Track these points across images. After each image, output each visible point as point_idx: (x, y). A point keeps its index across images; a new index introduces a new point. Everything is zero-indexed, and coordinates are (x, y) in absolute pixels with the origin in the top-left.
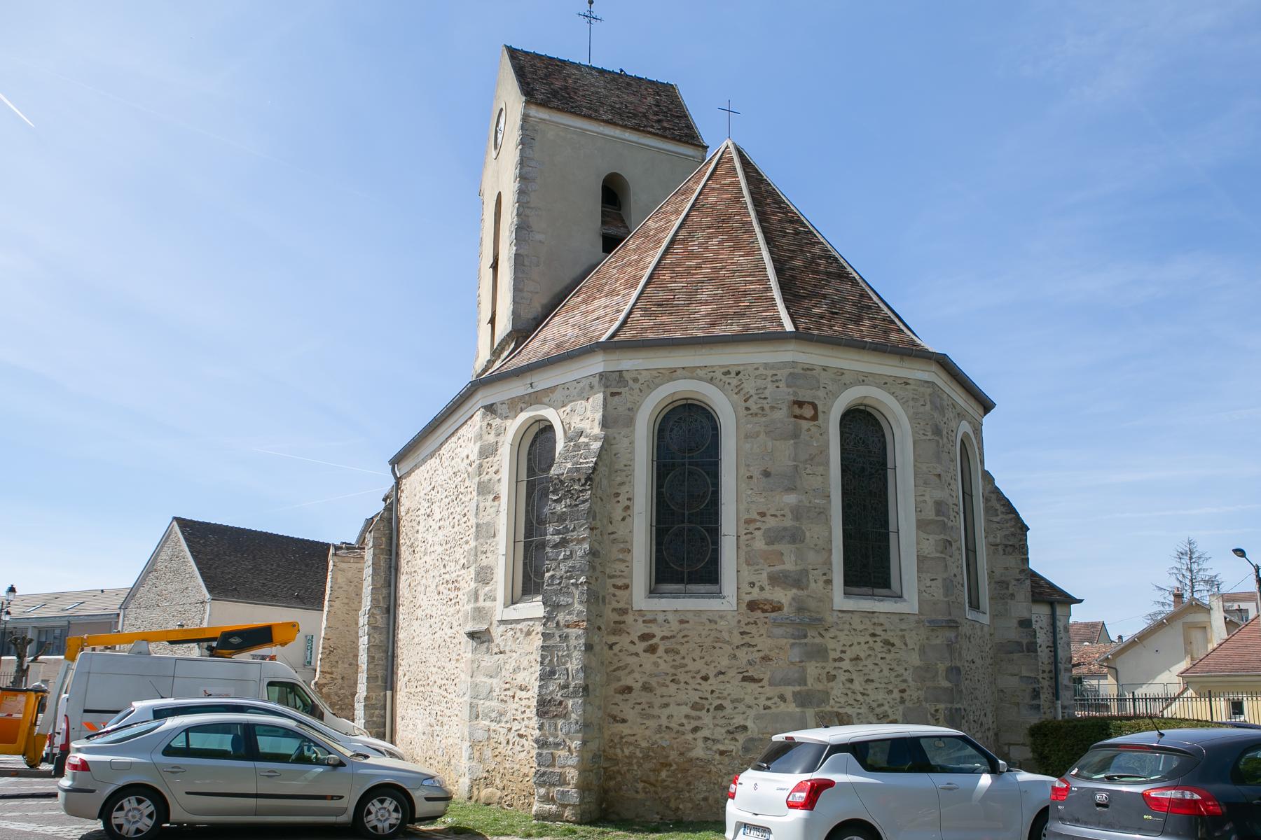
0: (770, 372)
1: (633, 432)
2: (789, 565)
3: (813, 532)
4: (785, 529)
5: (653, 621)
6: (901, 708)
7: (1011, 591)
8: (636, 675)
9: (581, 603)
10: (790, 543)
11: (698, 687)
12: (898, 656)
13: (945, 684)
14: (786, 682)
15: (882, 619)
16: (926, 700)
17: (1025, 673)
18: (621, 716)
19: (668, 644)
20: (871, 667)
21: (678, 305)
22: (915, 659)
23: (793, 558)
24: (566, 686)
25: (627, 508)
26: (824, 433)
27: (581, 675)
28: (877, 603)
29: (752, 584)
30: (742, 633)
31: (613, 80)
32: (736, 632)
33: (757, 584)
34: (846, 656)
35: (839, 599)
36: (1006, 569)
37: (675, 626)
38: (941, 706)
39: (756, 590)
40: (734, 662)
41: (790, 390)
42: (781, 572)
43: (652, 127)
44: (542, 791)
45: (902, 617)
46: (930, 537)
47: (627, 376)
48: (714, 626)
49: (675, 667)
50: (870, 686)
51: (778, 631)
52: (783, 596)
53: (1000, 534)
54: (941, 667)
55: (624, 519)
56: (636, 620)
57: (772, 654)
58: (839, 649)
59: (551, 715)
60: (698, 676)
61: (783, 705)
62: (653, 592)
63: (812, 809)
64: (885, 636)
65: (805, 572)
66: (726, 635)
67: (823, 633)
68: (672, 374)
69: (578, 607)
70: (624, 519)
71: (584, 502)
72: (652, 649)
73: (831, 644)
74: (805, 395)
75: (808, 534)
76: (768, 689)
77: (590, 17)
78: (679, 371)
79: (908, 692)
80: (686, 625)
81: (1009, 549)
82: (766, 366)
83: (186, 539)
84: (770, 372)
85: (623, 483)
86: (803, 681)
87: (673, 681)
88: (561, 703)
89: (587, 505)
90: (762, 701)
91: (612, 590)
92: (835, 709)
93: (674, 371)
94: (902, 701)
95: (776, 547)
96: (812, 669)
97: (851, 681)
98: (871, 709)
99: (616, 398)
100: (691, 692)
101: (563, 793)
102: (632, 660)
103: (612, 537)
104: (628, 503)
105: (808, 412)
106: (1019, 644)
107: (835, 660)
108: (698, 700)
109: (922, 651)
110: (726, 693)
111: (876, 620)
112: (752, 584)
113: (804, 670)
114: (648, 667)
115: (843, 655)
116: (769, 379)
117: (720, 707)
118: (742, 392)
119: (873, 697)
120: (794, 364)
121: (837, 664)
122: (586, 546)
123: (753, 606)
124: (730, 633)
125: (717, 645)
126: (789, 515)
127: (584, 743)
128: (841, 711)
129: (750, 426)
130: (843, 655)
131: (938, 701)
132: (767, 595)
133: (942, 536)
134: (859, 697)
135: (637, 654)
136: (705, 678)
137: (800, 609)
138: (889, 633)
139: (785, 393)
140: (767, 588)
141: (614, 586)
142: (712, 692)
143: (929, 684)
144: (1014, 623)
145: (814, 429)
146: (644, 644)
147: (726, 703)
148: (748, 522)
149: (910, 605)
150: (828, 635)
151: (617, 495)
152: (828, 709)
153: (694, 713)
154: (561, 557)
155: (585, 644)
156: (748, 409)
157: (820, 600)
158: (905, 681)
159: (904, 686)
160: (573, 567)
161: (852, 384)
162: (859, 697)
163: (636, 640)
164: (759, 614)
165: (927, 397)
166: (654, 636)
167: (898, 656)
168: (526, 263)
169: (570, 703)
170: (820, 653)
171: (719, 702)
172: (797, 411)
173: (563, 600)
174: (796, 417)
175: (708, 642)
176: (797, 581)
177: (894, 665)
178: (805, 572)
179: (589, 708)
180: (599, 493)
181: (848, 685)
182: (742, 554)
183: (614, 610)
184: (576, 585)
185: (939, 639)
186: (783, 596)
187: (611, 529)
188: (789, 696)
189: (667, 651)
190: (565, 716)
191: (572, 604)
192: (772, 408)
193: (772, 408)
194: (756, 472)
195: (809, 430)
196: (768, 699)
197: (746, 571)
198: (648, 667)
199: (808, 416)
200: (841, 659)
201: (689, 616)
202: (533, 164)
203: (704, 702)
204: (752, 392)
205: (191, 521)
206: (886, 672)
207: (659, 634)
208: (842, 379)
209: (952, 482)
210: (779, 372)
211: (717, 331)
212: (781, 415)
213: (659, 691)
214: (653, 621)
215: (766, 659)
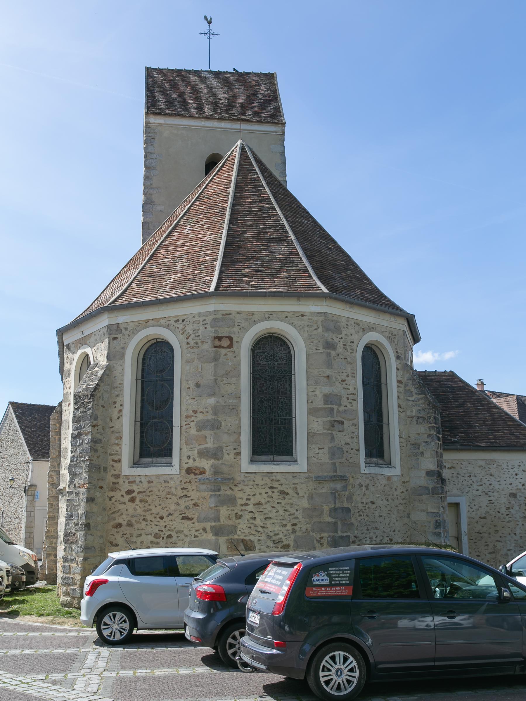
0: (201, 319)
1: (124, 362)
2: (210, 444)
3: (227, 422)
4: (208, 421)
5: (134, 482)
6: (292, 536)
7: (421, 450)
8: (124, 516)
9: (86, 472)
10: (210, 430)
11: (158, 523)
12: (291, 501)
13: (330, 520)
14: (207, 520)
15: (279, 477)
16: (313, 531)
17: (430, 510)
18: (115, 542)
19: (141, 496)
20: (269, 509)
21: (160, 276)
22: (305, 503)
23: (212, 440)
24: (76, 524)
25: (120, 411)
26: (237, 356)
27: (84, 517)
28: (274, 466)
29: (189, 457)
30: (182, 489)
31: (226, 79)
32: (179, 488)
33: (192, 457)
34: (251, 502)
35: (245, 464)
36: (419, 434)
37: (145, 485)
38: (325, 535)
39: (191, 461)
40: (177, 507)
41: (213, 330)
42: (205, 448)
43: (245, 114)
44: (64, 589)
45: (294, 475)
46: (320, 420)
47: (122, 327)
48: (167, 485)
49: (145, 511)
50: (268, 523)
51: (203, 487)
52: (206, 464)
53: (415, 409)
54: (326, 508)
55: (118, 418)
56: (124, 482)
57: (199, 502)
58: (245, 497)
59: (70, 542)
60: (158, 517)
61: (205, 535)
62: (135, 464)
63: (91, 596)
64: (280, 488)
65: (220, 449)
66: (173, 490)
67: (233, 487)
68: (146, 323)
69: (85, 475)
70: (118, 418)
71: (89, 409)
72: (133, 500)
73: (239, 495)
74: (224, 332)
75: (223, 423)
76: (197, 524)
77: (209, 34)
78: (151, 322)
79: (299, 526)
80: (151, 484)
81: (421, 420)
82: (199, 314)
83: (17, 417)
84: (201, 319)
85: (118, 395)
86: (217, 519)
87: (144, 520)
88: (75, 534)
89: (91, 411)
90: (194, 533)
91: (112, 463)
92: (242, 537)
93: (147, 321)
94: (294, 531)
95: (203, 433)
96: (224, 511)
97: (254, 518)
98: (269, 537)
99: (115, 341)
100: (154, 527)
101: (74, 590)
102: (122, 507)
103: (112, 429)
104: (120, 408)
105: (225, 343)
106: (426, 488)
107: (242, 505)
108: (158, 532)
109: (311, 497)
110: (173, 527)
111: (274, 478)
112: (189, 457)
113: (218, 512)
114: (131, 511)
115: (248, 502)
116: (201, 323)
117: (170, 536)
118: (186, 333)
119: (270, 529)
120: (216, 312)
121: (243, 508)
122: (89, 437)
123: (189, 471)
124: (176, 488)
125: (169, 496)
126: (211, 412)
127: (85, 559)
128: (245, 538)
129: (189, 355)
130: (248, 502)
131: (323, 531)
132: (197, 464)
133: (329, 418)
134: (260, 529)
135: (124, 503)
136: (162, 518)
137: (216, 473)
138: (284, 486)
139: (210, 332)
140: (197, 459)
141: (113, 460)
142: (166, 526)
143: (316, 520)
144: (423, 473)
145: (230, 354)
146: (128, 497)
147: (173, 534)
148: (187, 417)
149: (301, 466)
150: (236, 489)
151: (115, 403)
152: (236, 537)
153: (155, 540)
154: (78, 444)
155: (87, 498)
156: (188, 344)
157: (231, 466)
158: (296, 518)
159: (295, 521)
160: (83, 450)
161: (260, 321)
162: (260, 529)
163: (124, 494)
164: (192, 476)
165: (320, 323)
166: (134, 491)
167: (291, 501)
168: (151, 227)
169: (79, 534)
170: (231, 501)
171: (169, 533)
172: (217, 343)
173: (78, 471)
174: (216, 347)
175: (164, 495)
176: (215, 454)
177: (288, 507)
178: (220, 449)
179: (90, 538)
180: (101, 402)
181: (252, 521)
182: (183, 437)
183: (112, 475)
184: (83, 461)
185: (326, 489)
186: (206, 464)
187: (111, 424)
188: (208, 529)
189: (141, 501)
190: (76, 543)
191: (82, 473)
192: (202, 342)
193: (202, 342)
194: (192, 385)
195: (226, 354)
196: (197, 531)
197: (185, 449)
198: (131, 511)
199: (225, 345)
200: (247, 504)
201: (153, 479)
202: (154, 156)
203: (161, 533)
204: (191, 332)
205: (22, 404)
206: (281, 512)
207: (137, 490)
208: (251, 318)
209: (349, 380)
210: (207, 318)
211: (173, 294)
212: (207, 346)
213: (136, 526)
214: (134, 482)
215: (196, 505)
